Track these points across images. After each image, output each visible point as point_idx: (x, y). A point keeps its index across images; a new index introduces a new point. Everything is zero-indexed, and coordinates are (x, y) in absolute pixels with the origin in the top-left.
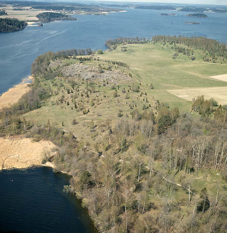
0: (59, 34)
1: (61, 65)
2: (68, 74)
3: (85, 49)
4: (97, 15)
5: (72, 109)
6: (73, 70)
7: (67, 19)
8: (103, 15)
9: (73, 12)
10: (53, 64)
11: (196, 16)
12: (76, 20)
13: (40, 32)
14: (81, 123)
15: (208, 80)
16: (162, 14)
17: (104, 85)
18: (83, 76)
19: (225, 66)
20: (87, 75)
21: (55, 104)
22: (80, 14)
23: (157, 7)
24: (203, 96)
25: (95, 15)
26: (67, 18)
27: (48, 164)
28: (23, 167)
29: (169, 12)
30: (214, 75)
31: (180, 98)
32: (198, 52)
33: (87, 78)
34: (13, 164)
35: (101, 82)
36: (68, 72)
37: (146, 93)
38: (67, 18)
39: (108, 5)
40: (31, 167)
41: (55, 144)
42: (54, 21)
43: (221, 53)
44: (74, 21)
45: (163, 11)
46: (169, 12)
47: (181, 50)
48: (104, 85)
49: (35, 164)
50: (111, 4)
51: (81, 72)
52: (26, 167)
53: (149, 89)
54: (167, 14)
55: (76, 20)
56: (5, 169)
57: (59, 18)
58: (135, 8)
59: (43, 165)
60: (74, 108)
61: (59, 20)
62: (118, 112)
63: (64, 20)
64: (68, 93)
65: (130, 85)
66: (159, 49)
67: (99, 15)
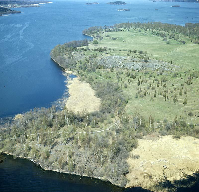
2: (110, 66)
6: (114, 62)
7: (13, 13)
9: (9, 5)
11: (116, 4)
54: (91, 3)
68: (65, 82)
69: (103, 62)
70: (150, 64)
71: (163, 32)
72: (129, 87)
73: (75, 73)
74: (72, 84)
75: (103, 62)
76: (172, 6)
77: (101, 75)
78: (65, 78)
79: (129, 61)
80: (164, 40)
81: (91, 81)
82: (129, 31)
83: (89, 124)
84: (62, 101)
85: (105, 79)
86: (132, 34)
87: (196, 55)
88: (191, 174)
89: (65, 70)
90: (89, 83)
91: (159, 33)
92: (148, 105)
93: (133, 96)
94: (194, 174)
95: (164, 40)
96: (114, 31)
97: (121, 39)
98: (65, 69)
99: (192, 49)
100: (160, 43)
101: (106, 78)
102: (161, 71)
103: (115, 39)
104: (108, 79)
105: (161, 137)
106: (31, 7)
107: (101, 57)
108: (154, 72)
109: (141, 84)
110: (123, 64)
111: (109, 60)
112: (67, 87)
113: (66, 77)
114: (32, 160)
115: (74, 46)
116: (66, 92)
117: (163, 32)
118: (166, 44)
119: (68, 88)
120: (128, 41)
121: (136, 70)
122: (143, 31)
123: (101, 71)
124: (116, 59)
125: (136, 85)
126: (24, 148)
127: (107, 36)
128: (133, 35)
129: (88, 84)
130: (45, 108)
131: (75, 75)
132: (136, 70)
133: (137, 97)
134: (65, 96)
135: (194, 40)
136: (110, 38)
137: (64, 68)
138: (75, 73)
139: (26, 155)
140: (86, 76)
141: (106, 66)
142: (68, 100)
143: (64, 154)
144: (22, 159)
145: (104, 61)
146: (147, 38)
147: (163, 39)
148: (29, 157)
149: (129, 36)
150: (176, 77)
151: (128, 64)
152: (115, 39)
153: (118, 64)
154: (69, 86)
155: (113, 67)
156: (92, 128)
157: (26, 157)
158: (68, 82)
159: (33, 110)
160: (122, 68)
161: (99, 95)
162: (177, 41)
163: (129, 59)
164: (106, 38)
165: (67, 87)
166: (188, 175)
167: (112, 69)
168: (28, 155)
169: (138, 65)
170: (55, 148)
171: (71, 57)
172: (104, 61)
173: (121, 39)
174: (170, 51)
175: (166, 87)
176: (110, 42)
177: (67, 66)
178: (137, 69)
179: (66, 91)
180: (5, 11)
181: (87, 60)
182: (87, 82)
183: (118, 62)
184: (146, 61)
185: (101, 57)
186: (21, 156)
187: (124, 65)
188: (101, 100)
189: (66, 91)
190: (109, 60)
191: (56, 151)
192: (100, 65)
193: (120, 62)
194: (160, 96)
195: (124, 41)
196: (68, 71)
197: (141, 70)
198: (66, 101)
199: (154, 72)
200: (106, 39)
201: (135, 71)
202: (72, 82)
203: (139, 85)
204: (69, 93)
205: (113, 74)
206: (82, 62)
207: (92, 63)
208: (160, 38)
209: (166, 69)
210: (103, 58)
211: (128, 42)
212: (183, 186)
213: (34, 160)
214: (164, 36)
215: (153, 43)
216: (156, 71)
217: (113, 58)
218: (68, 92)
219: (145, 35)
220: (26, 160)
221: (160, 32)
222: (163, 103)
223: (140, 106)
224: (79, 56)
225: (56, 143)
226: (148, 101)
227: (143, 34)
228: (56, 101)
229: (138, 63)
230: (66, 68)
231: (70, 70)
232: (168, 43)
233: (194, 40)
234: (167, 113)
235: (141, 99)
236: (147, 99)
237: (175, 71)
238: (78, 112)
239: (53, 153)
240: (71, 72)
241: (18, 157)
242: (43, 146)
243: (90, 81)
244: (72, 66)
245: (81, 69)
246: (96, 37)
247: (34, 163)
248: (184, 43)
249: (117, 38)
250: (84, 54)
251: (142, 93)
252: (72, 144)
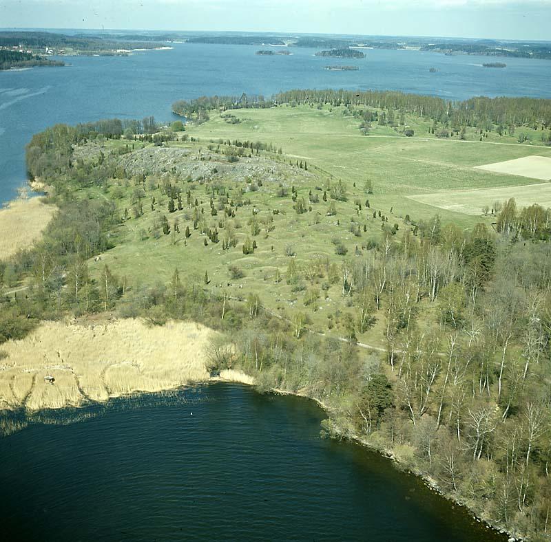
0: (32, 95)
1: (107, 153)
3: (140, 119)
4: (107, 55)
5: (206, 245)
6: (154, 161)
7: (41, 65)
8: (123, 55)
9: (47, 49)
10: (87, 152)
12: (63, 65)
13: (9, 92)
14: (249, 273)
15: (476, 174)
16: (261, 52)
17: (253, 189)
18: (186, 172)
19: (492, 146)
20: (196, 169)
21: (148, 238)
22: (66, 55)
23: (241, 38)
24: (512, 200)
25: (103, 55)
26: (41, 63)
27: (227, 375)
28: (164, 388)
29: (272, 47)
30: (481, 164)
31: (447, 210)
32: (412, 121)
33: (199, 176)
34: (131, 383)
35: (241, 182)
36: (138, 167)
37: (367, 201)
38: (41, 63)
39: (119, 37)
40: (186, 387)
41: (215, 328)
42: (9, 68)
43: (44, 179)
44: (60, 69)
45: (264, 47)
46: (272, 47)
47: (370, 118)
48: (253, 189)
49: (194, 378)
50: (122, 34)
51: (175, 163)
52: (171, 387)
53: (364, 194)
55: (63, 65)
56: (117, 398)
57: (20, 62)
58: (187, 41)
59: (216, 378)
60: (209, 242)
61: (21, 66)
62: (151, 242)
63: (33, 66)
64: (171, 212)
65: (320, 187)
66: (314, 117)
67: (111, 55)
70: (237, 165)
76: (485, 65)
88: (103, 397)
94: (110, 398)
103: (237, 122)
106: (103, 55)
118: (360, 136)
128: (291, 116)
135: (441, 127)
152: (237, 122)
153: (162, 166)
166: (91, 400)
169: (205, 168)
178: (200, 178)
180: (23, 59)
183: (165, 162)
209: (272, 179)
212: (48, 421)
237: (294, 183)
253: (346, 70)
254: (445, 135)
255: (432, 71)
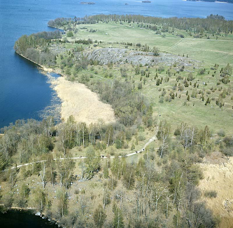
2: (107, 61)
6: (111, 56)
32: (177, 31)
68: (48, 82)
69: (96, 56)
71: (153, 25)
72: (146, 88)
73: (58, 71)
74: (58, 85)
75: (96, 56)
76: (143, 2)
77: (96, 73)
78: (44, 78)
79: (132, 54)
80: (156, 34)
81: (85, 82)
82: (107, 23)
83: (111, 142)
84: (53, 109)
85: (105, 78)
86: (114, 27)
87: (206, 50)
89: (42, 67)
90: (84, 83)
91: (147, 26)
92: (184, 112)
93: (157, 100)
95: (156, 34)
96: (88, 23)
97: (102, 32)
98: (41, 66)
99: (196, 43)
100: (154, 36)
101: (106, 77)
102: (181, 67)
103: (94, 31)
104: (108, 77)
105: (228, 159)
107: (88, 51)
108: (171, 69)
109: (161, 83)
110: (125, 59)
111: (104, 53)
112: (53, 89)
113: (46, 76)
114: (39, 214)
115: (47, 38)
116: (53, 95)
117: (153, 25)
119: (55, 91)
120: (112, 34)
121: (145, 66)
122: (126, 24)
123: (96, 68)
124: (114, 52)
125: (154, 85)
126: (17, 191)
127: (82, 28)
128: (115, 28)
129: (83, 85)
130: (35, 121)
131: (58, 73)
132: (145, 66)
133: (161, 102)
134: (55, 102)
136: (87, 30)
137: (39, 65)
138: (58, 71)
139: (21, 204)
140: (75, 74)
141: (101, 61)
142: (61, 108)
143: (92, 198)
144: (18, 211)
145: (96, 55)
146: (134, 32)
147: (155, 32)
148: (30, 208)
149: (110, 29)
150: (204, 75)
151: (132, 58)
152: (94, 31)
153: (118, 59)
154: (56, 88)
155: (112, 62)
156: (118, 148)
157: (24, 209)
158: (53, 83)
159: (14, 124)
160: (124, 63)
161: (106, 99)
162: (173, 34)
163: (132, 53)
164: (82, 30)
165: (53, 89)
167: (110, 65)
168: (27, 203)
170: (74, 187)
171: (46, 51)
172: (96, 55)
173: (102, 32)
174: (171, 46)
175: (198, 87)
176: (89, 35)
177: (44, 62)
178: (146, 65)
179: (55, 95)
181: (71, 54)
182: (79, 82)
184: (156, 55)
185: (88, 51)
186: (15, 207)
187: (126, 60)
188: (111, 106)
189: (55, 95)
190: (104, 53)
191: (77, 192)
192: (91, 60)
193: (121, 56)
194: (195, 100)
195: (106, 34)
196: (47, 68)
197: (152, 66)
198: (60, 110)
199: (171, 69)
200: (83, 32)
201: (144, 67)
202: (58, 82)
203: (158, 84)
204: (59, 98)
205: (114, 71)
206: (64, 57)
207: (80, 58)
208: (151, 31)
209: (187, 65)
210: (95, 51)
211: (113, 35)
213: (41, 213)
214: (155, 29)
215: (145, 36)
216: (173, 67)
217: (109, 51)
218: (58, 96)
219: (130, 28)
220: (24, 213)
221: (149, 24)
222: (204, 109)
223: (173, 114)
224: (55, 49)
225: (73, 179)
226: (181, 106)
227: (127, 27)
228: (43, 109)
229: (146, 56)
230: (42, 64)
231: (49, 67)
232: (164, 36)
233: (193, 34)
234: (217, 123)
235: (168, 104)
236: (178, 103)
238: (84, 124)
239: (72, 197)
240: (51, 70)
241: (8, 208)
242: (49, 184)
243: (84, 81)
244: (52, 62)
245: (65, 66)
246: (68, 29)
247: (43, 218)
248: (182, 37)
249: (96, 30)
250: (65, 47)
251: (167, 95)
252: (100, 178)
253: (90, 4)
254: (197, 37)
255: (126, 4)
